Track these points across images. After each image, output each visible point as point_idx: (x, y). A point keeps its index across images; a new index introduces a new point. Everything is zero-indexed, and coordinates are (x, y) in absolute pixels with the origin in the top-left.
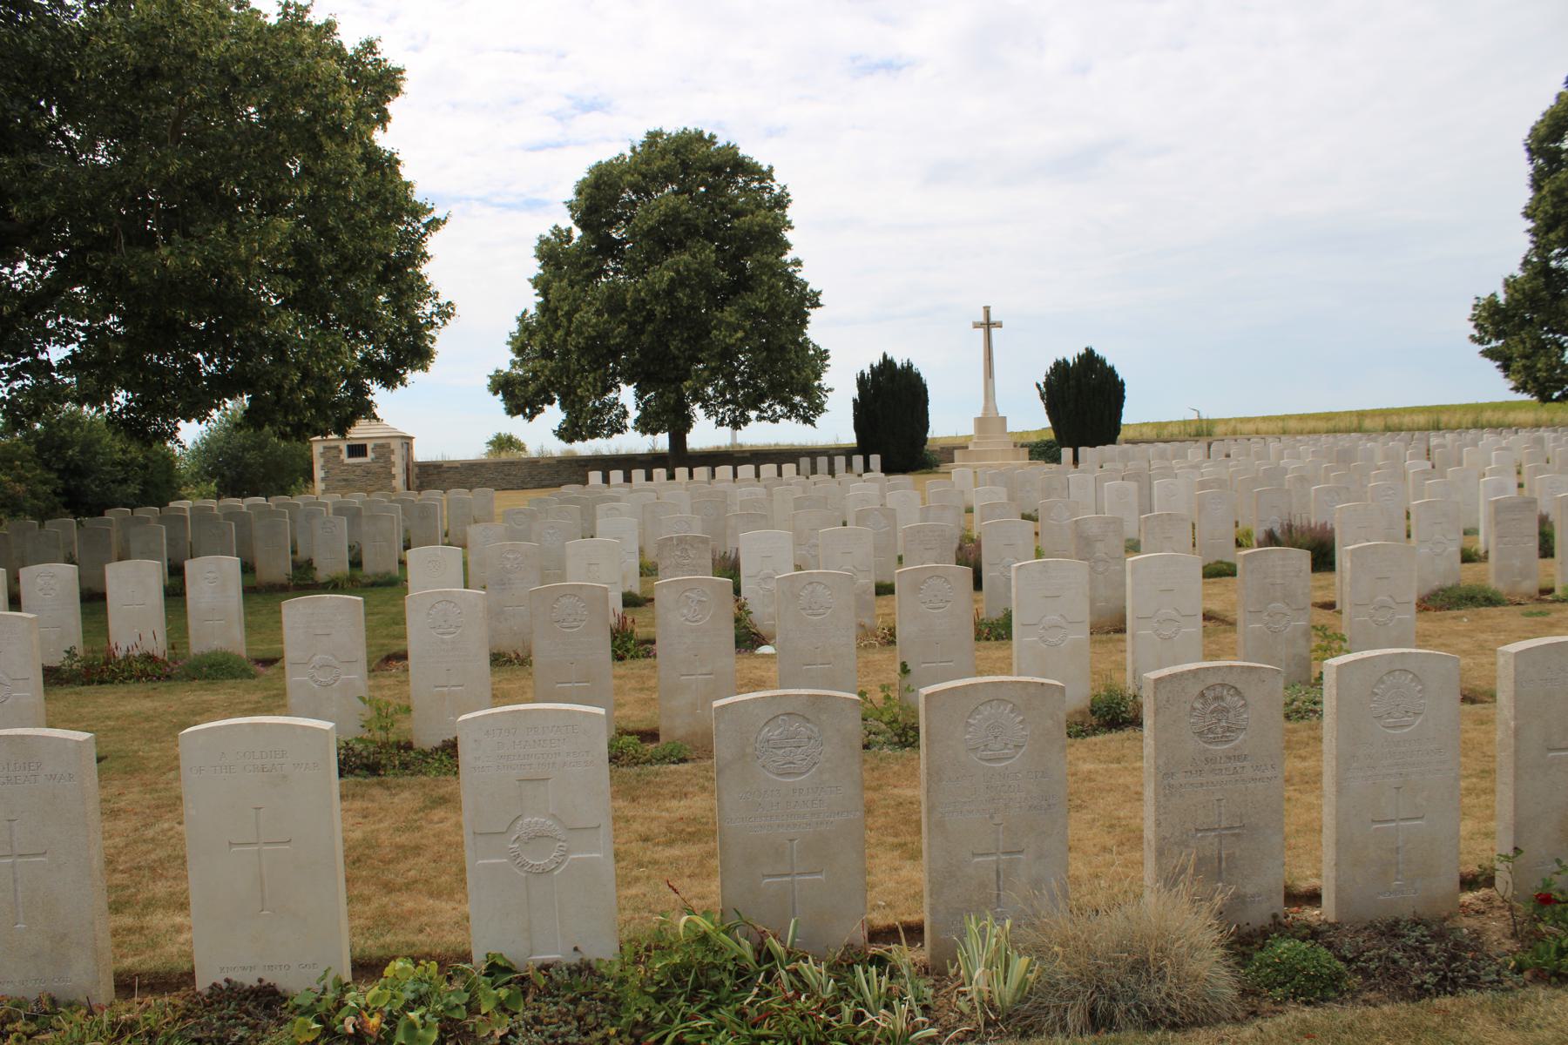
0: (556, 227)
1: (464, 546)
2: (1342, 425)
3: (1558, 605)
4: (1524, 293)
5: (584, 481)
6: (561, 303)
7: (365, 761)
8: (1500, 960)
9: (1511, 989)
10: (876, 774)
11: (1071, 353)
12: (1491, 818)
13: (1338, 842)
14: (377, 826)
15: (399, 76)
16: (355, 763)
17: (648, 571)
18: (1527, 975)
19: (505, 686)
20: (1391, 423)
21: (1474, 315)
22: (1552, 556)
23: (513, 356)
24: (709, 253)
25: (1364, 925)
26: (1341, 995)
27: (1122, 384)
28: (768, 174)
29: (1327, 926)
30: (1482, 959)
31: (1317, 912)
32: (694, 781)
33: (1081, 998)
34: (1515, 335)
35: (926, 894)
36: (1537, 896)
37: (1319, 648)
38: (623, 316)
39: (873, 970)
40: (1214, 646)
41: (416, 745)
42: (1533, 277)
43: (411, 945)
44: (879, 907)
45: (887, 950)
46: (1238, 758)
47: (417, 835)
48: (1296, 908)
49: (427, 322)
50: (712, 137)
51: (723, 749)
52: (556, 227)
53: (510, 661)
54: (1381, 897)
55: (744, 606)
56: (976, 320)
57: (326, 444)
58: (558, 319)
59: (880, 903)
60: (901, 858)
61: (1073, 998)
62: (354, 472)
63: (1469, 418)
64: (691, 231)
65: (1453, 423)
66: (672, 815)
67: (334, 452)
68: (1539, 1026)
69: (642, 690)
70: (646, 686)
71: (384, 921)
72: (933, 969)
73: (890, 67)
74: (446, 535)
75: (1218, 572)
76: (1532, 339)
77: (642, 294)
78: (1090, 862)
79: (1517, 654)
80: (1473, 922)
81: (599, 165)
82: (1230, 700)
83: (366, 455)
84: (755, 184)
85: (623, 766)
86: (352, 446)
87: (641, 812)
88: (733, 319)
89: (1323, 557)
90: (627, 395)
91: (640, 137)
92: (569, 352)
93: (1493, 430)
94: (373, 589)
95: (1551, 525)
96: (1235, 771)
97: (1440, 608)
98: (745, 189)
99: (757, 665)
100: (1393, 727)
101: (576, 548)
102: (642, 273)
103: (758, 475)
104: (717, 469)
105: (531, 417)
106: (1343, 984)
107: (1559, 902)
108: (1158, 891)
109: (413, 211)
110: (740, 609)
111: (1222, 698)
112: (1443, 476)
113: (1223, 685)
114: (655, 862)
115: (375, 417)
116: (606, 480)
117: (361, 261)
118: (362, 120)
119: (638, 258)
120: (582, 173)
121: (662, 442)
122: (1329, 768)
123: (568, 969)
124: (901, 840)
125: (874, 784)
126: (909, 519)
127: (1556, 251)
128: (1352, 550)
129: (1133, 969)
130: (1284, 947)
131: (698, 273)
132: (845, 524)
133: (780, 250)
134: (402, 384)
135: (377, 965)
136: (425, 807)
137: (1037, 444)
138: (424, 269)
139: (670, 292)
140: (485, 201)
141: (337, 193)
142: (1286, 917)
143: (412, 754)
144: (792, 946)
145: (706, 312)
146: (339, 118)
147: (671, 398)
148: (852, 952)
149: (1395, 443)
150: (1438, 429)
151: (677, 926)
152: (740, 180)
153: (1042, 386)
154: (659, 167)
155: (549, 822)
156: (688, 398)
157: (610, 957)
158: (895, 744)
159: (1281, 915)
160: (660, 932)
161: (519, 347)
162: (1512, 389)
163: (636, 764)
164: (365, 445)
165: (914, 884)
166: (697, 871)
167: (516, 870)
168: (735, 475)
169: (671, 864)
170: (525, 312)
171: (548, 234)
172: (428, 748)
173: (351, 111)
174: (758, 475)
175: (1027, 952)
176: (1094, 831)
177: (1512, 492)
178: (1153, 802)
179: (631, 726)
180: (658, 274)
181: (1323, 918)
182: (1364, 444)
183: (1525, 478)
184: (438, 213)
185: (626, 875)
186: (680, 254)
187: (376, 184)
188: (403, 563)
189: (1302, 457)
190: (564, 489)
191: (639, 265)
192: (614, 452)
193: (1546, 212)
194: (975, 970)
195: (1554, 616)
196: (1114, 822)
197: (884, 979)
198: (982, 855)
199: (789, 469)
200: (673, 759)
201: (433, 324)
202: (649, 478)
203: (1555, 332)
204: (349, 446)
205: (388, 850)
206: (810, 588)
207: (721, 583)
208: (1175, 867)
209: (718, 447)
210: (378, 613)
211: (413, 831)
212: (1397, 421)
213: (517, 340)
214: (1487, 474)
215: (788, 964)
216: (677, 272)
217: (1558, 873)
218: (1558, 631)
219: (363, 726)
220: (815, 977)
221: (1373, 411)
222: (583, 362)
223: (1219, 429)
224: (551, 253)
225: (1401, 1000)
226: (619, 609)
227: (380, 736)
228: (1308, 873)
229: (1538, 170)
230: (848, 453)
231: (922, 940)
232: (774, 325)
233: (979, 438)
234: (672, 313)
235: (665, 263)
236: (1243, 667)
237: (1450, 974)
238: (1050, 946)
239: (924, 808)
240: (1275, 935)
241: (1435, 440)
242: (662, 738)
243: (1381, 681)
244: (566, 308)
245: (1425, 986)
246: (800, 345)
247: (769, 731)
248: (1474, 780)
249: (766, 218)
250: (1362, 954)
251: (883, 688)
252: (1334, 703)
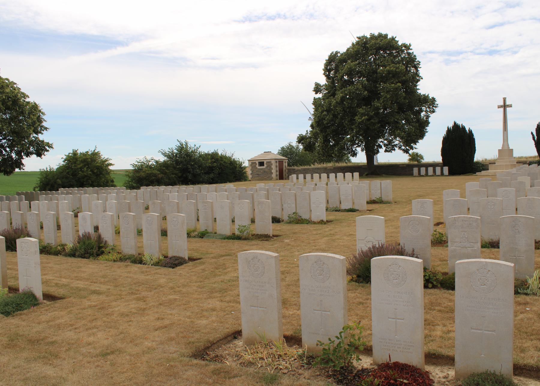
56: (499, 104)
62: (260, 171)
86: (260, 162)
153: (535, 134)
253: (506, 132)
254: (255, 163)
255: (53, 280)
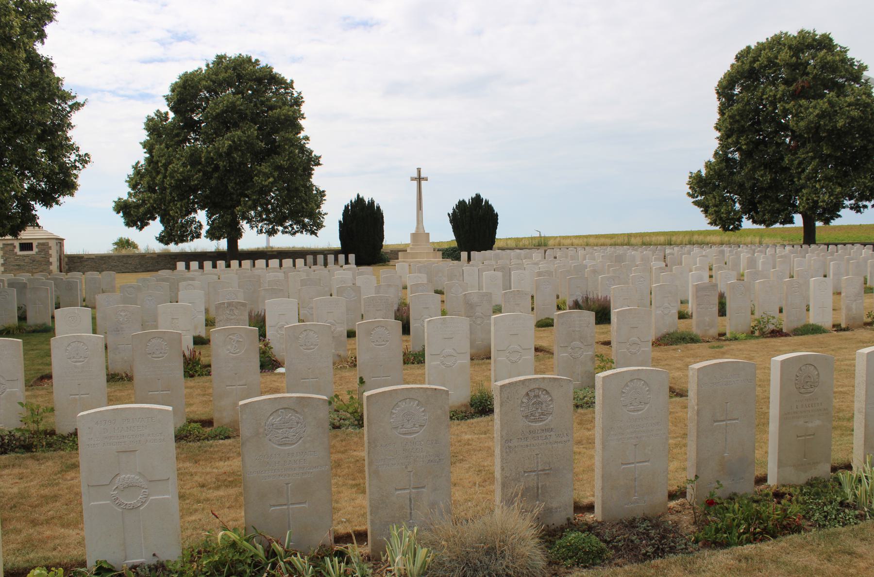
0: (158, 111)
1: (94, 308)
2: (619, 241)
3: (727, 342)
4: (715, 171)
5: (174, 268)
6: (161, 158)
7: (22, 443)
8: (687, 537)
9: (692, 552)
10: (344, 443)
11: (467, 197)
12: (686, 460)
13: (603, 476)
14: (29, 484)
15: (52, 9)
16: (15, 444)
17: (210, 323)
18: (700, 544)
19: (118, 394)
20: (645, 241)
21: (690, 181)
22: (725, 315)
23: (130, 190)
24: (253, 131)
25: (617, 522)
26: (603, 562)
27: (497, 215)
28: (290, 85)
29: (597, 524)
30: (678, 537)
31: (592, 516)
32: (234, 450)
33: (457, 571)
34: (710, 193)
35: (368, 514)
36: (706, 501)
37: (599, 367)
38: (199, 167)
39: (336, 559)
40: (542, 367)
41: (57, 432)
42: (718, 163)
43: (46, 559)
44: (342, 522)
45: (345, 548)
46: (547, 430)
47: (56, 488)
48: (581, 514)
49: (72, 166)
50: (257, 61)
51: (245, 430)
52: (158, 111)
53: (122, 378)
54: (626, 506)
55: (268, 344)
57: (5, 242)
58: (158, 167)
59: (343, 520)
60: (356, 493)
61: (453, 571)
62: (24, 260)
63: (687, 239)
64: (243, 117)
65: (679, 241)
66: (220, 471)
67: (11, 247)
68: (704, 571)
69: (204, 395)
70: (207, 392)
71: (30, 544)
72: (373, 558)
73: (366, 24)
74: (84, 301)
75: (545, 324)
76: (719, 196)
77: (212, 154)
78: (466, 492)
79: (699, 369)
80: (674, 517)
81: (186, 74)
82: (543, 397)
83: (32, 250)
84: (283, 90)
85: (190, 442)
86: (23, 243)
87: (200, 470)
88: (267, 171)
89: (603, 315)
90: (201, 216)
91: (212, 58)
92: (165, 189)
93: (698, 245)
94: (35, 334)
95: (725, 298)
96: (546, 438)
97: (667, 345)
98: (276, 93)
99: (276, 380)
100: (633, 411)
101: (164, 309)
102: (212, 141)
103: (281, 265)
104: (256, 261)
105: (141, 228)
106: (604, 555)
107: (718, 504)
108: (502, 507)
109: (62, 96)
110: (265, 346)
111: (538, 396)
112: (671, 271)
113: (539, 389)
114: (208, 500)
115: (38, 225)
116: (188, 267)
117: (26, 126)
118: (26, 35)
119: (210, 132)
120: (175, 79)
121: (223, 244)
122: (598, 433)
123: (149, 568)
124: (357, 482)
125: (342, 449)
126: (369, 292)
127: (732, 149)
128: (618, 312)
129: (487, 553)
130: (572, 536)
131: (246, 142)
132: (331, 295)
133: (297, 131)
134: (57, 203)
135: (23, 573)
136: (62, 471)
137: (447, 249)
138: (70, 134)
139: (229, 154)
140: (113, 93)
141: (9, 81)
142: (575, 519)
143: (55, 437)
144: (288, 548)
145: (251, 167)
146: (9, 33)
147: (228, 218)
148: (324, 549)
149: (647, 252)
150: (671, 245)
151: (217, 539)
152: (273, 87)
154: (223, 77)
155: (137, 477)
156: (239, 218)
157: (176, 559)
158: (356, 425)
159: (572, 518)
160: (207, 542)
161: (134, 184)
162: (709, 224)
163: (198, 441)
164: (32, 244)
165: (364, 507)
166: (234, 504)
167: (117, 508)
168: (267, 265)
169: (218, 500)
170: (138, 163)
171: (153, 115)
172: (65, 433)
173: (18, 29)
174: (281, 265)
175: (425, 545)
176: (470, 474)
177: (706, 280)
178: (500, 456)
179: (196, 417)
180: (221, 143)
181: (595, 519)
182: (631, 252)
183: (713, 273)
184: (80, 99)
185: (189, 509)
186: (236, 131)
187: (36, 77)
188: (53, 317)
189: (597, 258)
190: (161, 272)
191: (210, 136)
192: (193, 250)
193: (727, 127)
194: (396, 557)
195: (725, 348)
196: (481, 468)
197: (343, 565)
198: (401, 489)
199: (300, 262)
200: (221, 437)
201: (76, 167)
202: (215, 266)
203: (730, 194)
204: (20, 244)
205: (35, 499)
206: (305, 333)
207: (251, 330)
208: (512, 494)
209: (258, 248)
210: (37, 350)
211: (53, 486)
212: (648, 240)
213: (132, 180)
214: (694, 269)
215: (285, 558)
216: (234, 141)
217: (717, 488)
218: (727, 356)
219: (21, 421)
220: (301, 564)
221: (637, 234)
222: (174, 194)
223: (551, 242)
224: (154, 127)
225: (635, 562)
226: (191, 346)
227: (33, 427)
228: (588, 494)
229: (722, 104)
230: (336, 253)
231: (367, 541)
232: (292, 175)
233: (413, 245)
234: (230, 166)
235: (226, 136)
236: (550, 378)
237: (661, 546)
238: (440, 541)
239: (366, 463)
240: (568, 530)
241: (668, 250)
242: (215, 424)
243: (627, 385)
244: (164, 161)
245: (648, 554)
246: (308, 188)
247: (273, 419)
248: (679, 439)
249: (288, 111)
250: (615, 538)
251: (349, 392)
252: (601, 398)
253: (421, 212)
254: (12, 244)
255: (760, 365)
